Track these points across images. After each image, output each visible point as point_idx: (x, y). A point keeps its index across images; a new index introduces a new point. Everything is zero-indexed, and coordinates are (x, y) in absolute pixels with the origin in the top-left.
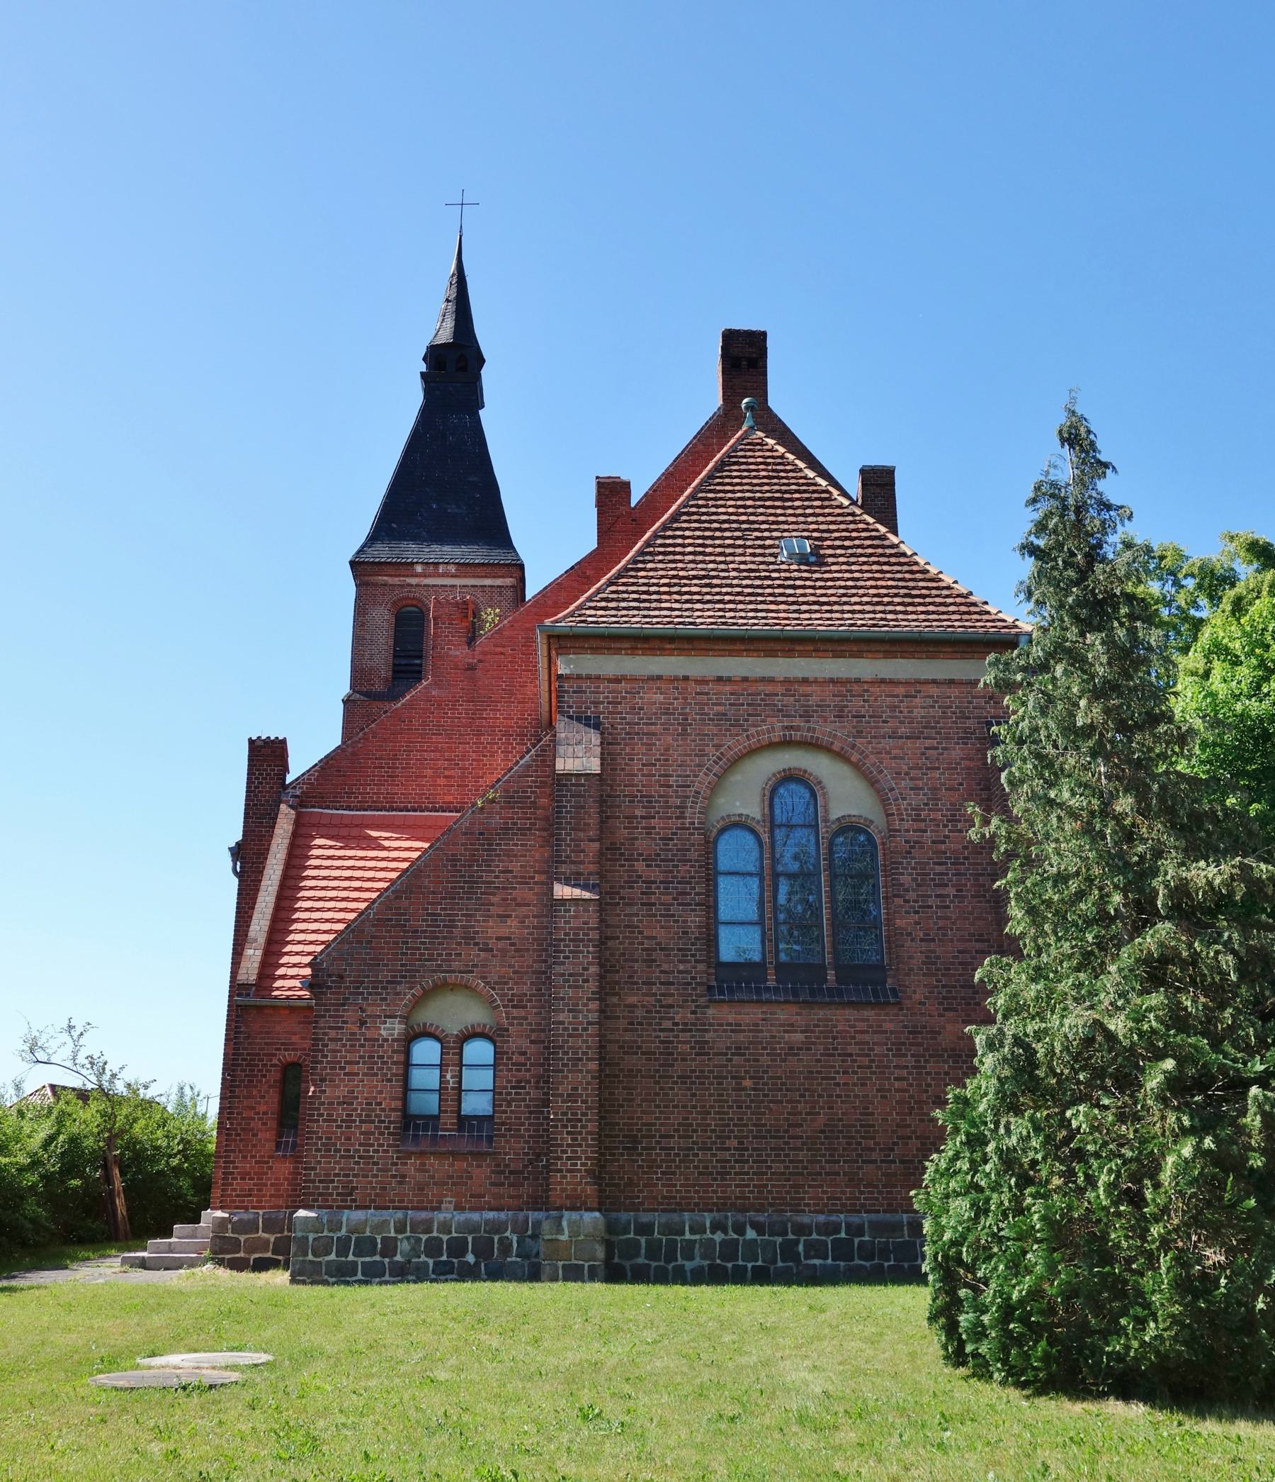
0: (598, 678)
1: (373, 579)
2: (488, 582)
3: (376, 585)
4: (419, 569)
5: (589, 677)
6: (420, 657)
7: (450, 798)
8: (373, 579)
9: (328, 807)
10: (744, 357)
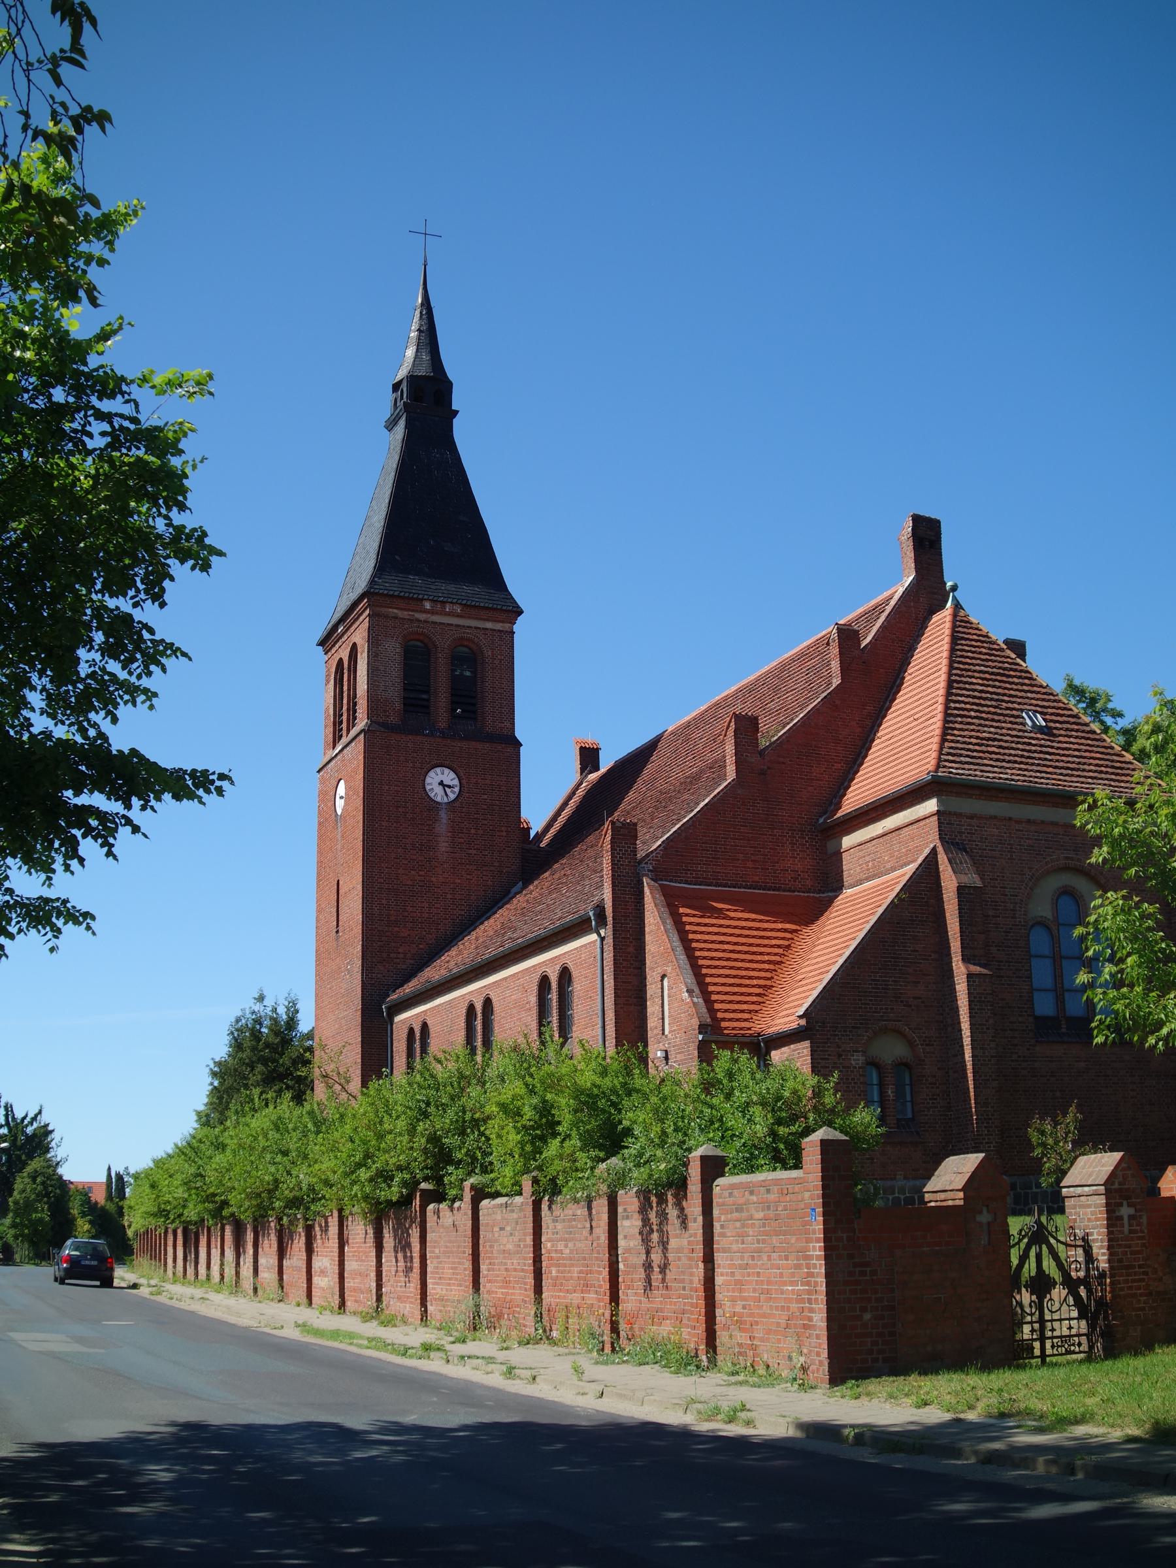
0: (961, 814)
1: (383, 610)
2: (489, 625)
3: (386, 617)
4: (428, 605)
5: (955, 814)
6: (427, 692)
7: (757, 878)
8: (383, 610)
9: (671, 881)
10: (926, 537)
